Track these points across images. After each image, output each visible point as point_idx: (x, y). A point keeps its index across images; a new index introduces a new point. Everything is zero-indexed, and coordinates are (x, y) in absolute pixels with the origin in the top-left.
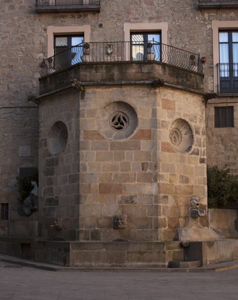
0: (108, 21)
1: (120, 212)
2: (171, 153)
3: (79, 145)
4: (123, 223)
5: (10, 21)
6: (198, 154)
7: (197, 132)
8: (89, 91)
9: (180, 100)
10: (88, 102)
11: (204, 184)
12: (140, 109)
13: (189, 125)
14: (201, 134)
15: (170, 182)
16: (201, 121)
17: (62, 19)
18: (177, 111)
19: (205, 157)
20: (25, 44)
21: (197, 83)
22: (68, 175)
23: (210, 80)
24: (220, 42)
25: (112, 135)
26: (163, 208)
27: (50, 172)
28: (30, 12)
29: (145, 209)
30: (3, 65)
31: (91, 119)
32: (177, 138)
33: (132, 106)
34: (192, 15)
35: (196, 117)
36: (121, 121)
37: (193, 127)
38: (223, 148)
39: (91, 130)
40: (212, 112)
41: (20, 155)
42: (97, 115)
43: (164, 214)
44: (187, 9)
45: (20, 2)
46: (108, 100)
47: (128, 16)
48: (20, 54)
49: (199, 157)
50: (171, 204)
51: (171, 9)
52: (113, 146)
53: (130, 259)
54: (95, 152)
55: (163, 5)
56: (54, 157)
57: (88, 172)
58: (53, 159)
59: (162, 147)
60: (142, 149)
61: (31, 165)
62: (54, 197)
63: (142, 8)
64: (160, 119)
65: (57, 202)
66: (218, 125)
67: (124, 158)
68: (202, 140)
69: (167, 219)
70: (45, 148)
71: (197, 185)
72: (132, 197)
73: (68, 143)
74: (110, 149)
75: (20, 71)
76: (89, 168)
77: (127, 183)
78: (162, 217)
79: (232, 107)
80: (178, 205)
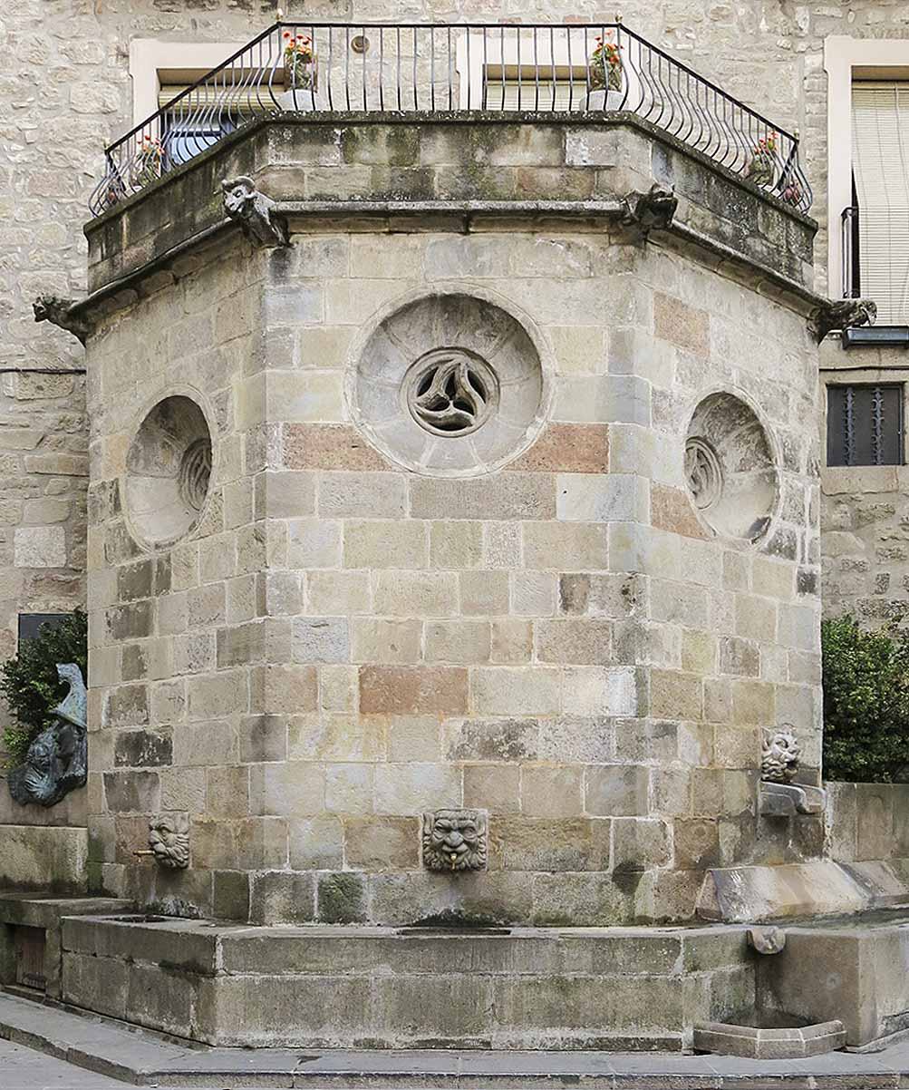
1: (456, 795)
3: (261, 493)
6: (791, 554)
10: (305, 297)
14: (803, 471)
15: (687, 662)
20: (35, 112)
21: (791, 257)
22: (212, 631)
27: (135, 623)
29: (577, 783)
31: (320, 372)
34: (742, 11)
36: (460, 393)
39: (321, 422)
41: (21, 564)
49: (795, 567)
52: (426, 495)
53: (508, 1013)
54: (341, 523)
57: (304, 614)
58: (148, 564)
61: (67, 606)
62: (150, 730)
65: (165, 749)
67: (477, 552)
68: (808, 499)
69: (670, 829)
70: (111, 522)
72: (512, 732)
73: (215, 484)
75: (16, 223)
76: (313, 600)
77: (494, 668)
78: (652, 818)
80: (717, 766)
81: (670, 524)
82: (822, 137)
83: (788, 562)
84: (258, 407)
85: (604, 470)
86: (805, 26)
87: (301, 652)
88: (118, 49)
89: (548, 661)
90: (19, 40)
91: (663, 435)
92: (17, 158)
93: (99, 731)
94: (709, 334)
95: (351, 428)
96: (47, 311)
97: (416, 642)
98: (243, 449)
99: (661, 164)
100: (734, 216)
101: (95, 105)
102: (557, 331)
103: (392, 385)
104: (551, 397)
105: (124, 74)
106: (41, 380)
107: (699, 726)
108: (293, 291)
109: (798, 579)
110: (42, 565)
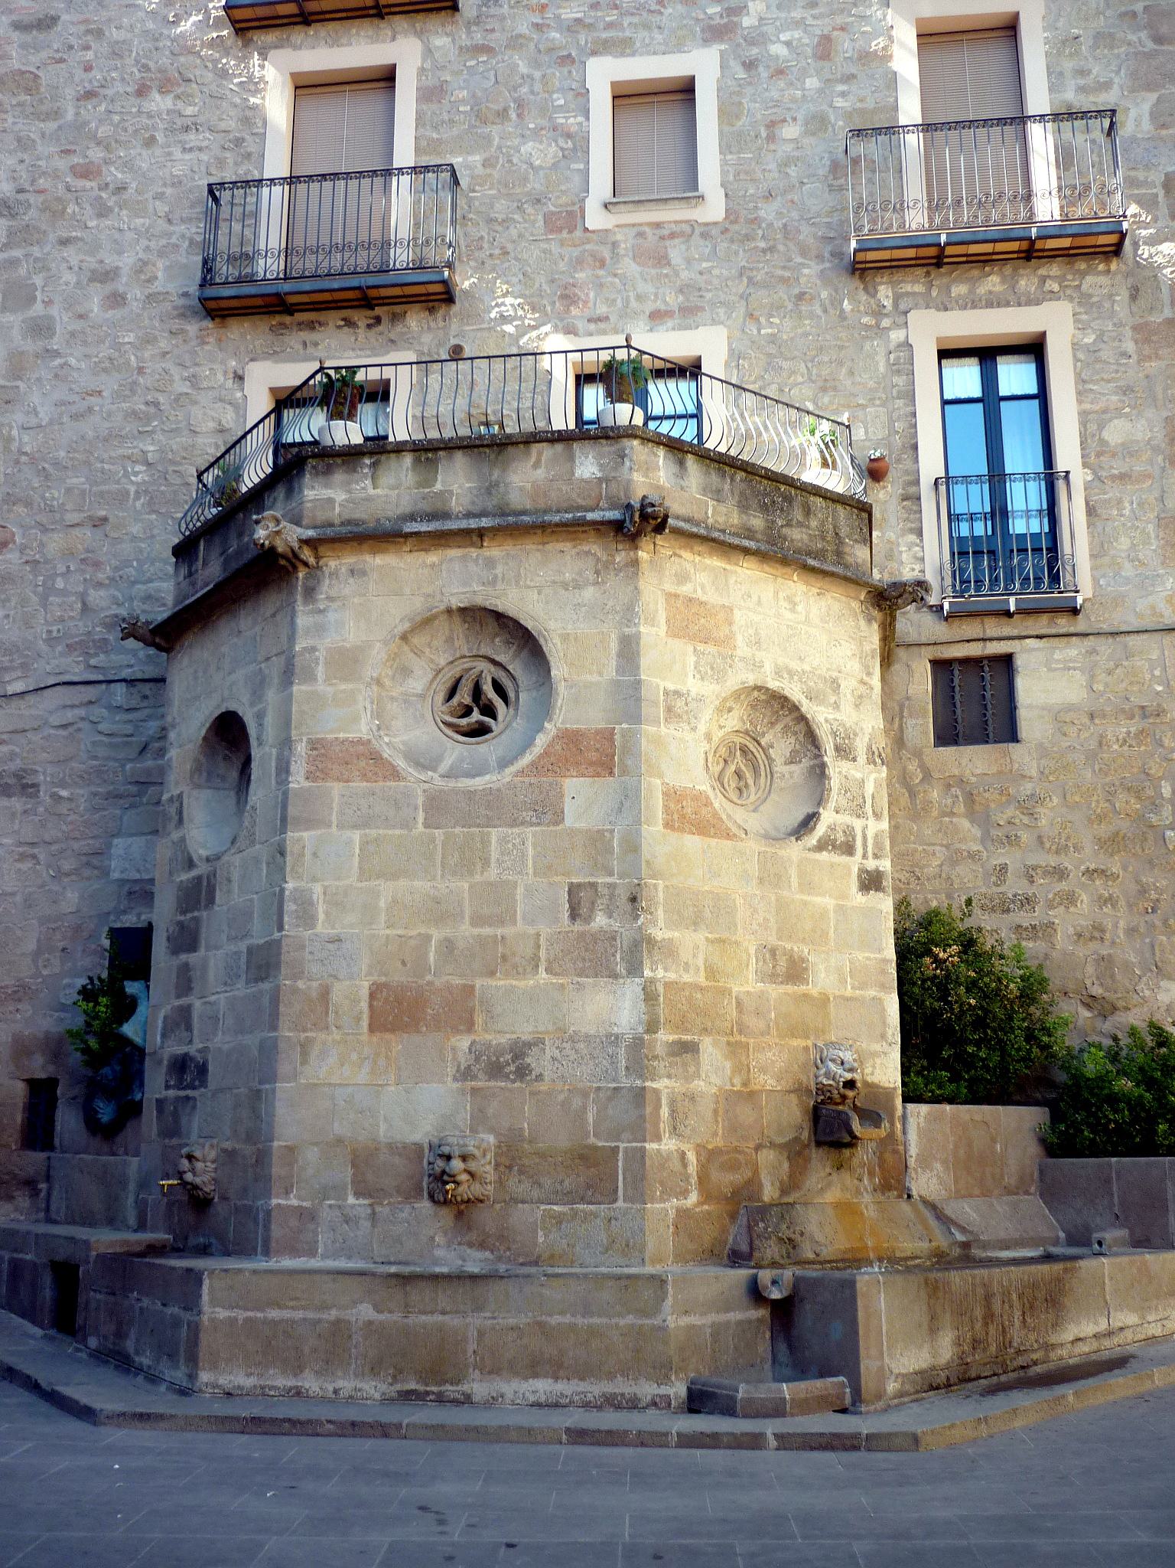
0: (485, 334)
1: (464, 1117)
2: (713, 842)
3: (284, 807)
4: (471, 1174)
5: (105, 351)
6: (848, 849)
7: (844, 752)
8: (337, 563)
9: (759, 603)
10: (332, 616)
11: (883, 987)
12: (565, 638)
13: (802, 719)
14: (862, 758)
15: (712, 972)
16: (859, 702)
17: (305, 335)
18: (742, 649)
19: (885, 865)
20: (159, 436)
23: (910, 547)
24: (948, 396)
25: (439, 759)
26: (672, 1103)
27: (187, 939)
28: (182, 316)
29: (584, 1108)
30: (72, 517)
31: (343, 687)
32: (749, 776)
33: (529, 625)
35: (835, 685)
37: (826, 727)
38: (977, 832)
39: (341, 735)
40: (921, 683)
41: (116, 875)
42: (369, 672)
43: (674, 1130)
44: (806, 271)
45: (148, 281)
46: (417, 605)
47: (568, 311)
48: (136, 474)
49: (854, 863)
50: (714, 1079)
51: (741, 275)
54: (356, 836)
55: (704, 265)
56: (202, 869)
58: (199, 878)
59: (666, 808)
60: (569, 821)
63: (623, 278)
64: (655, 680)
65: (202, 1070)
66: (948, 735)
67: (486, 862)
68: (870, 789)
69: (691, 1157)
70: (175, 836)
71: (849, 992)
72: (519, 1050)
74: (426, 826)
75: (134, 539)
76: (327, 914)
77: (500, 982)
78: (669, 1144)
79: (1007, 660)
81: (687, 827)
82: (910, 409)
83: (845, 859)
84: (286, 723)
85: (611, 773)
86: (888, 303)
87: (315, 969)
88: (235, 372)
89: (556, 974)
90: (148, 371)
91: (678, 734)
92: (139, 479)
93: (155, 1053)
94: (735, 628)
95: (369, 741)
96: (131, 630)
97: (426, 954)
98: (273, 764)
99: (674, 468)
100: (764, 508)
101: (211, 425)
102: (565, 638)
103: (414, 695)
104: (560, 702)
105: (239, 395)
106: (146, 689)
107: (728, 1043)
108: (321, 611)
109: (859, 876)
110: (137, 876)
